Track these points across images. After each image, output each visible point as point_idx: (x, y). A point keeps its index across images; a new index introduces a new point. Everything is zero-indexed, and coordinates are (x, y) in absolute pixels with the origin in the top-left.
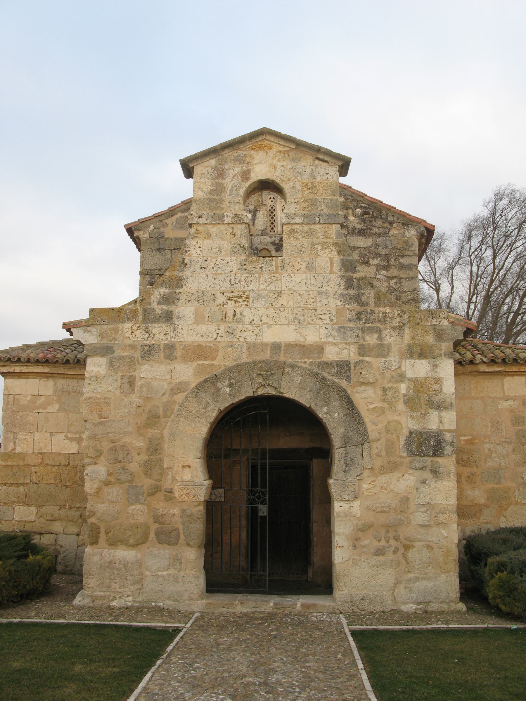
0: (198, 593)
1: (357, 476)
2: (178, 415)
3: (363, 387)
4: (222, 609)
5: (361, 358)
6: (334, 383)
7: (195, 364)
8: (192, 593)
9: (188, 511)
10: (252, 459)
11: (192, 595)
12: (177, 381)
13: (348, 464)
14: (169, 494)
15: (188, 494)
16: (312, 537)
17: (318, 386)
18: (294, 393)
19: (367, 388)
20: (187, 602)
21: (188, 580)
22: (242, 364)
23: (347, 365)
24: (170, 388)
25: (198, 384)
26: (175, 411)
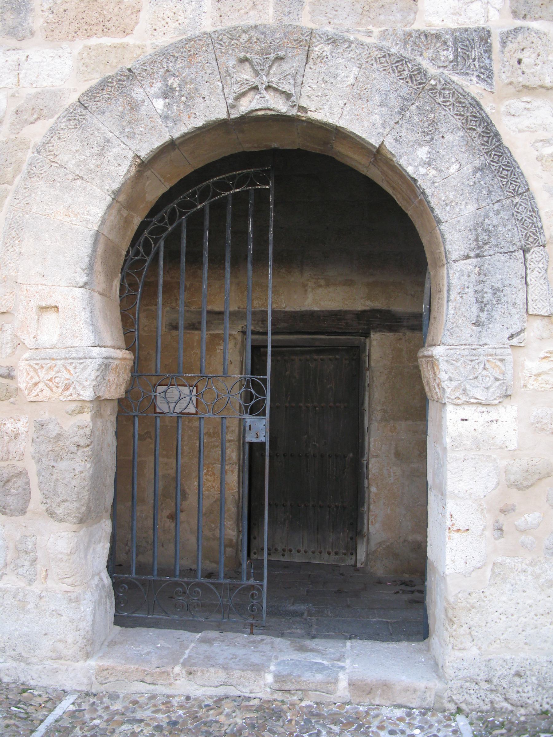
0: (75, 642)
1: (512, 337)
2: (30, 175)
3: (525, 99)
4: (140, 687)
5: (519, 23)
6: (447, 83)
7: (79, 45)
8: (60, 641)
9: (51, 426)
10: (254, 333)
11: (60, 646)
12: (33, 91)
13: (487, 303)
14: (6, 381)
15: (50, 380)
16: (366, 485)
17: (404, 91)
18: (337, 110)
19: (537, 102)
20: (50, 664)
21: (52, 607)
22: (199, 38)
23: (481, 39)
24: (13, 109)
25: (84, 94)
26: (25, 167)
